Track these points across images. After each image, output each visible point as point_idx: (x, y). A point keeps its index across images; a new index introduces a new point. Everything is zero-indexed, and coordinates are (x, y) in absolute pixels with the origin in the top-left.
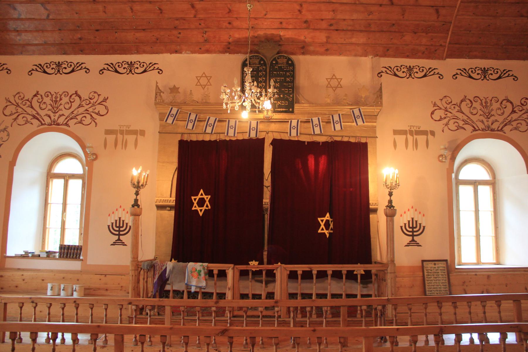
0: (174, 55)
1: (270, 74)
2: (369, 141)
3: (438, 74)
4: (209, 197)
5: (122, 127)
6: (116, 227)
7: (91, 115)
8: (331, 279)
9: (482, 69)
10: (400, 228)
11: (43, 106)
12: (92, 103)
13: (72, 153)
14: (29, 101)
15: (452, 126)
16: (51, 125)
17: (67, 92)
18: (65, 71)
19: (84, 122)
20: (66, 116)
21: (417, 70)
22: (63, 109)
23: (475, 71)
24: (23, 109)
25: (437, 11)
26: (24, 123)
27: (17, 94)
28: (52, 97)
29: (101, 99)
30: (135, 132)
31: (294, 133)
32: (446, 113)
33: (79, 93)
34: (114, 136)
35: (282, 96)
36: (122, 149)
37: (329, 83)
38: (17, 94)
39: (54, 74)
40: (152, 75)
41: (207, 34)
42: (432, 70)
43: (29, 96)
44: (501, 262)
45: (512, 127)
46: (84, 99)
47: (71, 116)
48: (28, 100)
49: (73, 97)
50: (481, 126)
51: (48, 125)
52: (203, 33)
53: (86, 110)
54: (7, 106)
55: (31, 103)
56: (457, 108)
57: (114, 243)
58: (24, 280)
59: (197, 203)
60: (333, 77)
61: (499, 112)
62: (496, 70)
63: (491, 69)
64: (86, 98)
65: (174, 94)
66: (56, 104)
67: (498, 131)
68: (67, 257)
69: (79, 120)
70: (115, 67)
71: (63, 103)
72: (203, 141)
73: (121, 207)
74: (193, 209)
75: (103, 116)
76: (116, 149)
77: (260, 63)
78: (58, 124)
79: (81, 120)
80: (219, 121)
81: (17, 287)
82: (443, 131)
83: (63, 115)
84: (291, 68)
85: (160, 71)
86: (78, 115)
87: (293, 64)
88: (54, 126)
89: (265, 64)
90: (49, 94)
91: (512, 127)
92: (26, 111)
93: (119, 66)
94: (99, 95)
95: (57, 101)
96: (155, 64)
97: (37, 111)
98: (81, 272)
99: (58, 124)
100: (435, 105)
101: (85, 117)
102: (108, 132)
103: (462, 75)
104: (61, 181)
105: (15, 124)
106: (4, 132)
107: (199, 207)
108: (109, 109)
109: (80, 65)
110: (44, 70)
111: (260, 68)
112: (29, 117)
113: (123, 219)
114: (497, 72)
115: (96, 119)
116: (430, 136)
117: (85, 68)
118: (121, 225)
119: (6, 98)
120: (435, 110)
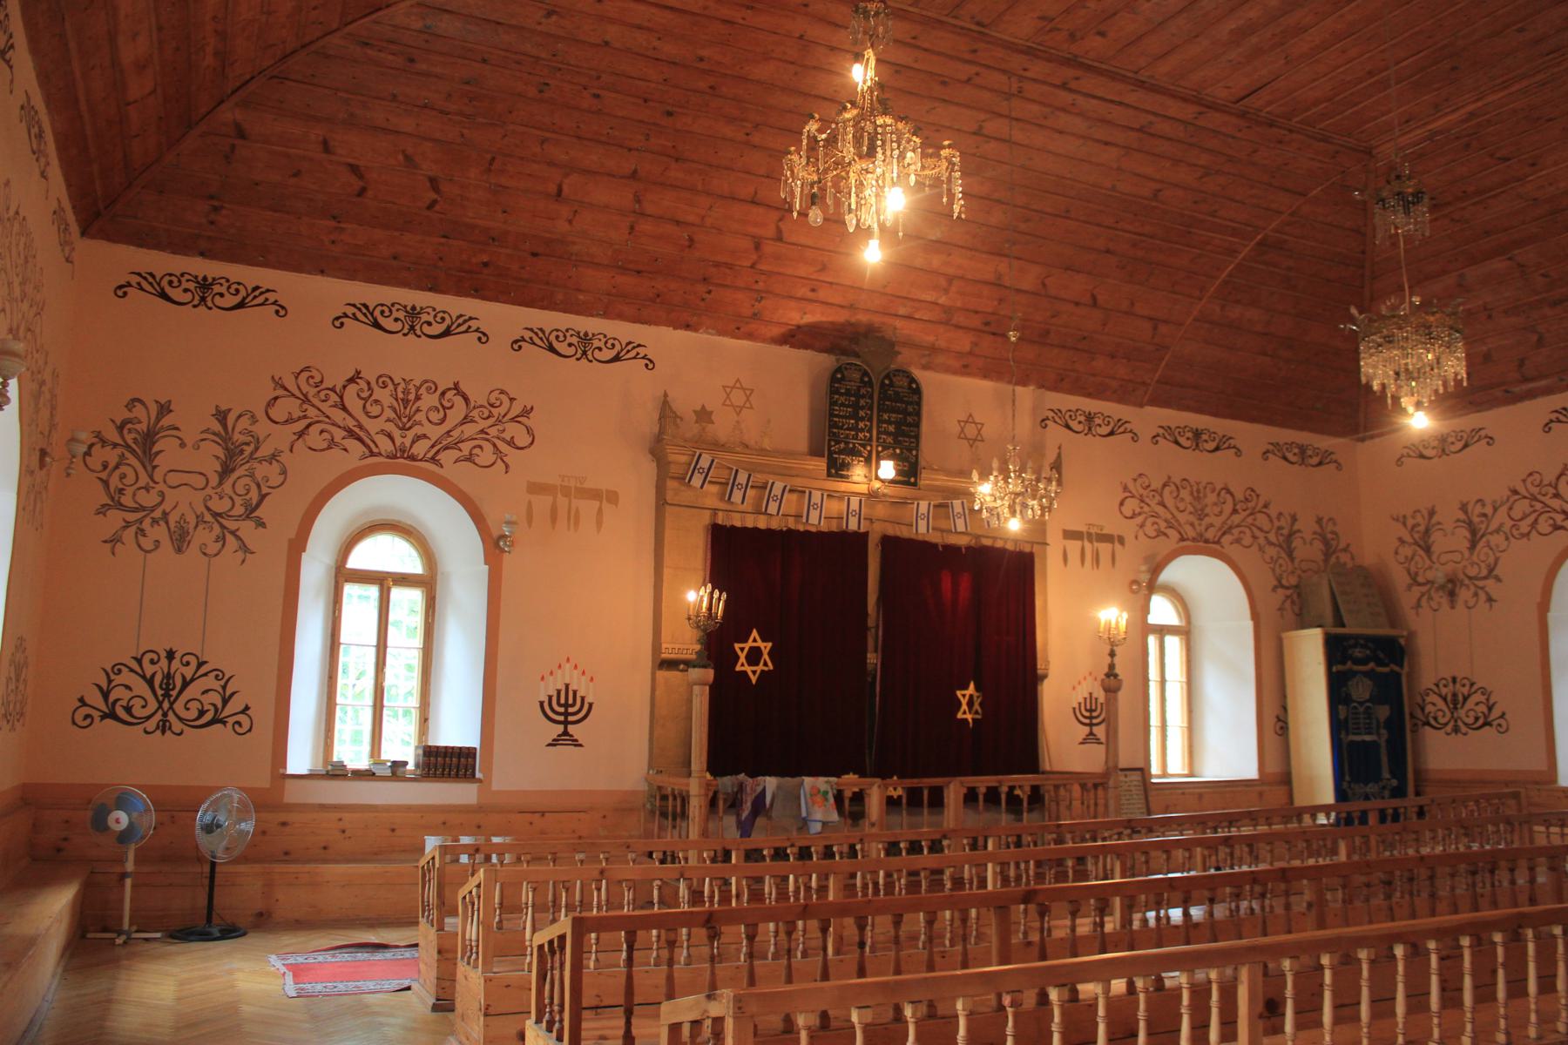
0: (681, 333)
1: (879, 404)
2: (1036, 549)
3: (275, 303)
4: (770, 644)
5: (566, 479)
6: (1086, 710)
7: (495, 445)
8: (929, 813)
9: (581, 335)
10: (1071, 710)
11: (375, 410)
12: (496, 415)
13: (399, 522)
14: (336, 392)
15: (1150, 529)
16: (395, 457)
17: (434, 383)
18: (426, 329)
19: (477, 460)
20: (434, 440)
21: (601, 344)
22: (425, 422)
23: (565, 336)
24: (319, 410)
25: (1155, 328)
26: (325, 445)
27: (302, 371)
28: (395, 390)
29: (516, 410)
30: (595, 495)
31: (922, 528)
32: (1142, 505)
33: (462, 387)
34: (550, 499)
35: (898, 451)
36: (569, 529)
37: (962, 431)
38: (302, 371)
39: (400, 334)
40: (631, 369)
41: (763, 302)
42: (262, 293)
43: (336, 378)
44: (1196, 773)
45: (459, 454)
46: (477, 405)
47: (444, 443)
48: (333, 390)
49: (449, 395)
50: (1191, 533)
51: (388, 457)
52: (756, 300)
53: (482, 431)
54: (276, 398)
55: (341, 397)
56: (1158, 498)
57: (554, 740)
58: (344, 832)
59: (746, 658)
60: (970, 419)
62: (611, 342)
63: (223, 281)
64: (479, 403)
65: (704, 424)
66: (405, 408)
67: (1214, 543)
68: (457, 775)
69: (466, 452)
70: (548, 340)
71: (424, 408)
72: (756, 529)
73: (568, 660)
74: (738, 668)
75: (522, 448)
76: (554, 528)
77: (862, 381)
78: (413, 458)
79: (471, 454)
80: (791, 491)
81: (325, 848)
82: (1136, 537)
83: (425, 436)
84: (915, 398)
85: (650, 364)
86: (463, 441)
87: (918, 391)
88: (402, 460)
89: (870, 384)
90: (388, 380)
91: (459, 454)
92: (328, 417)
93: (557, 337)
94: (512, 400)
95: (408, 401)
96: (639, 346)
97: (357, 421)
98: (479, 809)
99: (413, 458)
100: (1125, 489)
101: (480, 447)
102: (535, 488)
103: (142, 289)
104: (373, 591)
105: (299, 445)
106: (271, 463)
107: (749, 665)
108: (535, 433)
109: (465, 321)
110: (375, 319)
111: (863, 391)
112: (339, 434)
113: (575, 688)
114: (237, 291)
115: (506, 455)
116: (1117, 546)
118: (570, 701)
119: (273, 377)
120: (1126, 498)
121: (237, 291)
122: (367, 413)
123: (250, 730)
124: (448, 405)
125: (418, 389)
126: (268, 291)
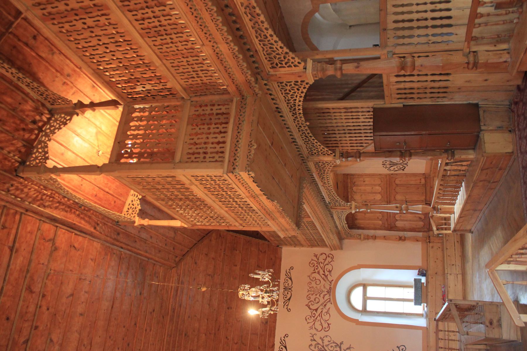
3: (290, 270)
11: (317, 300)
29: (315, 259)
45: (329, 275)
54: (315, 328)
61: (318, 282)
91: (329, 275)
104: (369, 302)
114: (287, 280)
117: (284, 338)
121: (287, 280)
122: (318, 302)
123: (404, 346)
124: (314, 279)
125: (310, 288)
126: (281, 339)
